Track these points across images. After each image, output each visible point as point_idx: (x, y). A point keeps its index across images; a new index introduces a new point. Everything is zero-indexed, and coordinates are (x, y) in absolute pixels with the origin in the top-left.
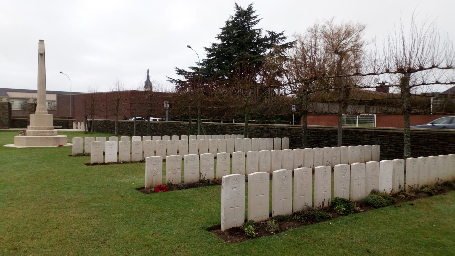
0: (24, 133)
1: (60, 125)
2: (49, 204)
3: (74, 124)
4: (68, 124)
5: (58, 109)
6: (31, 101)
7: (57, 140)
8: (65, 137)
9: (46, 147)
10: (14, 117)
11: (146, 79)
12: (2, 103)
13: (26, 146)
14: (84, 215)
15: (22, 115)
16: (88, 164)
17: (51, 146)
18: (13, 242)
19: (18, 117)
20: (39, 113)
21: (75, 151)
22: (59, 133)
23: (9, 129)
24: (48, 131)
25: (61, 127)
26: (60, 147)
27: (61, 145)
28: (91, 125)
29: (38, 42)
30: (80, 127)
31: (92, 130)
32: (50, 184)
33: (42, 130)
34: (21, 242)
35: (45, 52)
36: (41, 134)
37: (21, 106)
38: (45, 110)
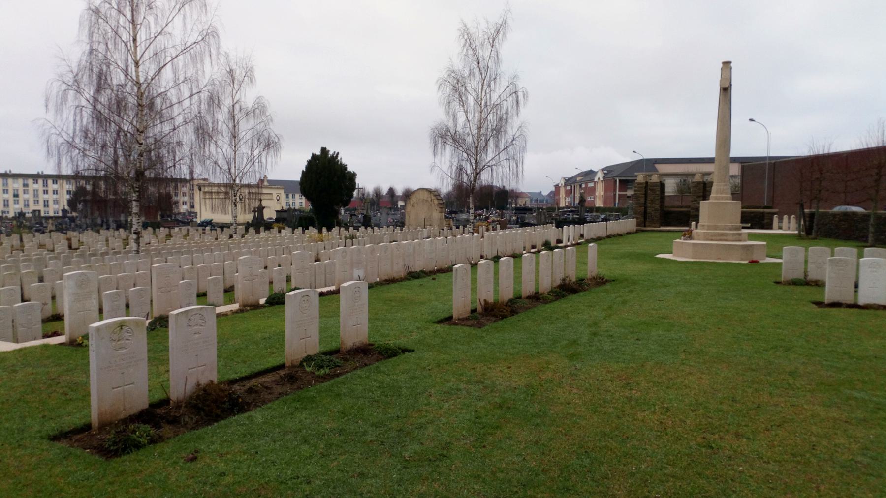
0: (689, 235)
2: (754, 373)
3: (776, 219)
4: (763, 220)
5: (742, 193)
6: (697, 178)
7: (748, 250)
8: (763, 245)
9: (727, 263)
12: (651, 183)
13: (693, 258)
14: (834, 413)
15: (677, 203)
16: (819, 304)
17: (735, 260)
18: (704, 432)
20: (716, 198)
21: (786, 274)
22: (752, 237)
24: (731, 232)
25: (749, 225)
26: (754, 264)
27: (754, 259)
28: (811, 221)
29: (721, 66)
30: (788, 226)
31: (813, 233)
32: (748, 335)
33: (720, 230)
34: (717, 436)
35: (732, 83)
36: (718, 238)
37: (676, 189)
38: (726, 193)
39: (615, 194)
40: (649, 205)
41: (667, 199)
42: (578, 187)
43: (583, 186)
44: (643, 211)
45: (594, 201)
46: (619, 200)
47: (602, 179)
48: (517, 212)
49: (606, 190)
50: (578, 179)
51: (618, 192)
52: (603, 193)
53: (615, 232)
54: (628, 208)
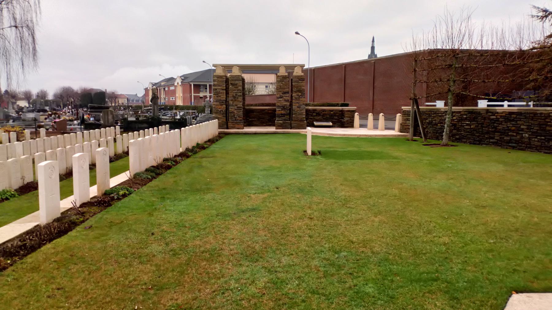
1: (327, 121)
3: (357, 116)
10: (248, 105)
11: (369, 52)
19: (252, 105)
23: (243, 129)
39: (191, 96)
40: (231, 102)
41: (186, 104)
42: (163, 89)
43: (166, 89)
44: (224, 110)
45: (175, 101)
46: (194, 100)
47: (180, 84)
48: (92, 110)
49: (184, 93)
50: (162, 84)
51: (193, 94)
52: (181, 95)
53: (191, 144)
54: (205, 106)
